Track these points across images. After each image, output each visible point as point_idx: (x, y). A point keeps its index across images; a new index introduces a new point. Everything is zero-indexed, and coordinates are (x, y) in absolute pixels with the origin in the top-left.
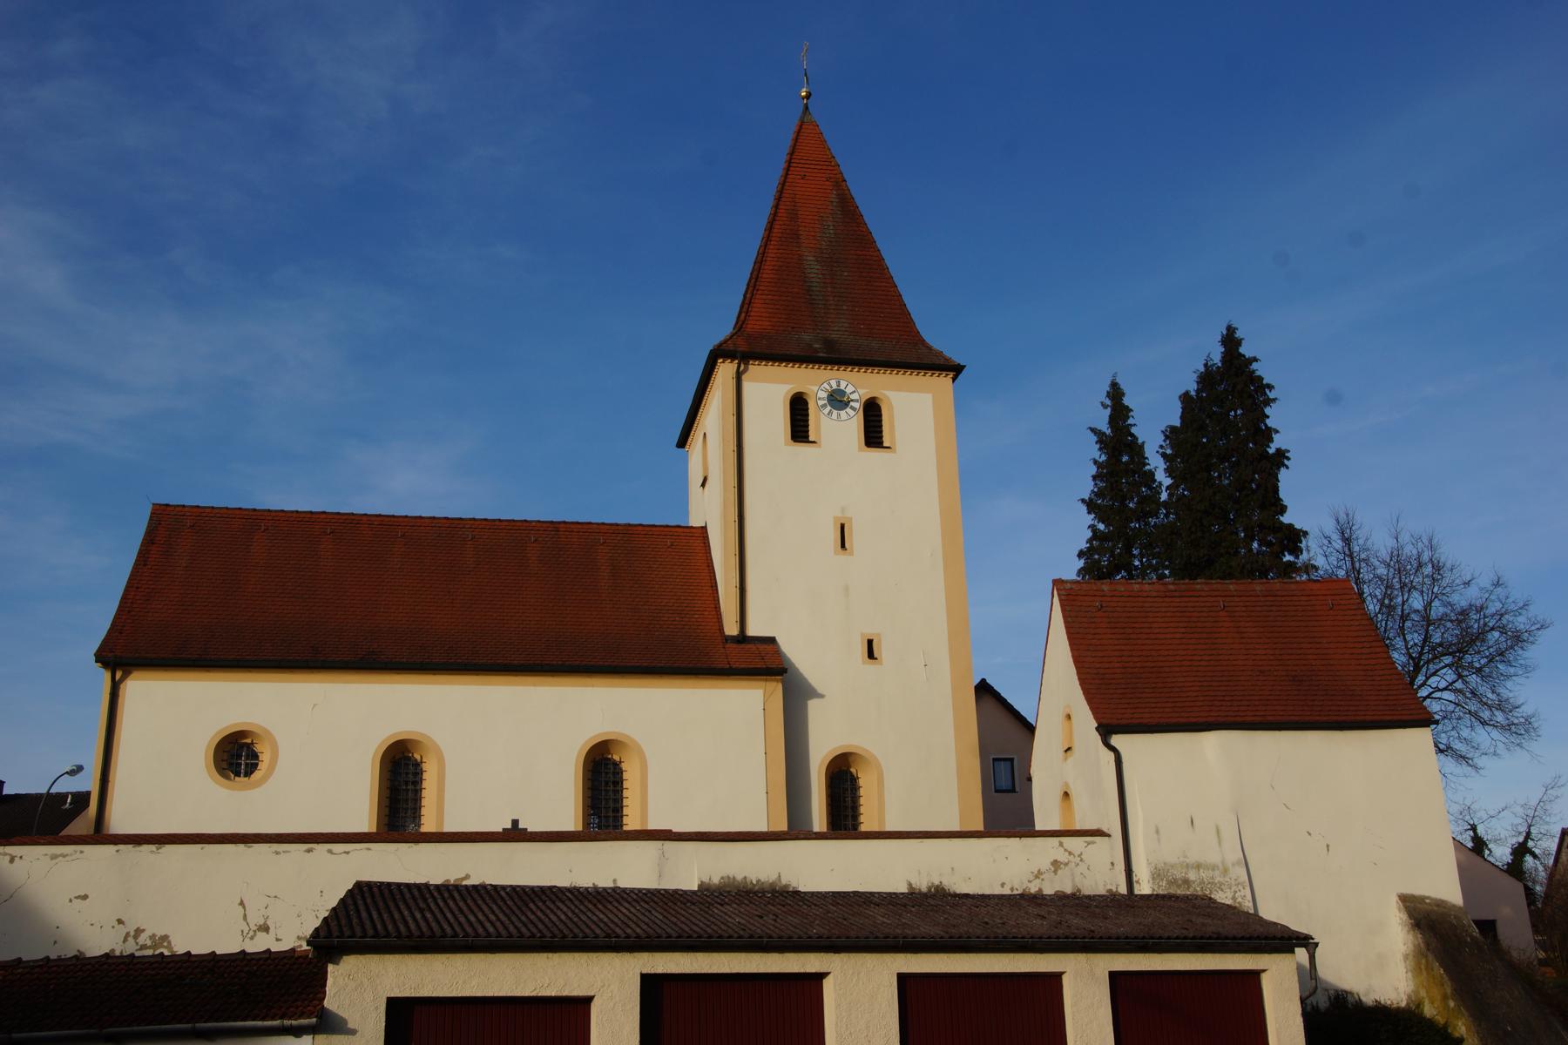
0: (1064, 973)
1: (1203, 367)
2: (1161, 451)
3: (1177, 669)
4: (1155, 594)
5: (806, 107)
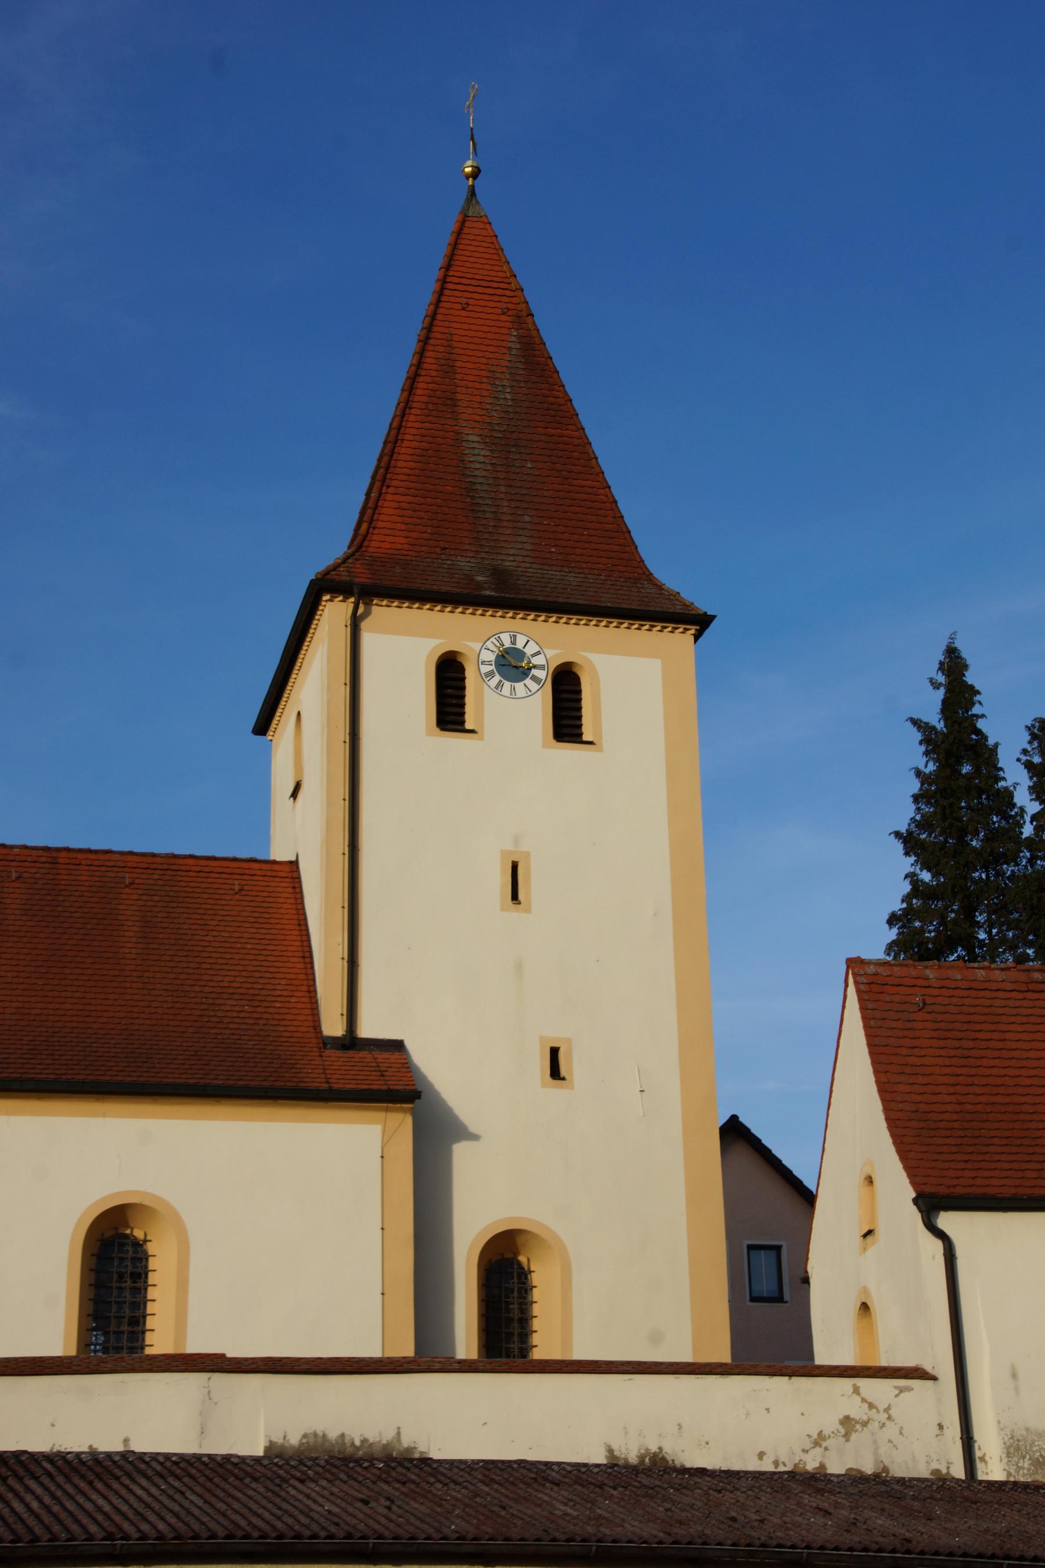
2: (1024, 758)
4: (1010, 987)
5: (472, 192)
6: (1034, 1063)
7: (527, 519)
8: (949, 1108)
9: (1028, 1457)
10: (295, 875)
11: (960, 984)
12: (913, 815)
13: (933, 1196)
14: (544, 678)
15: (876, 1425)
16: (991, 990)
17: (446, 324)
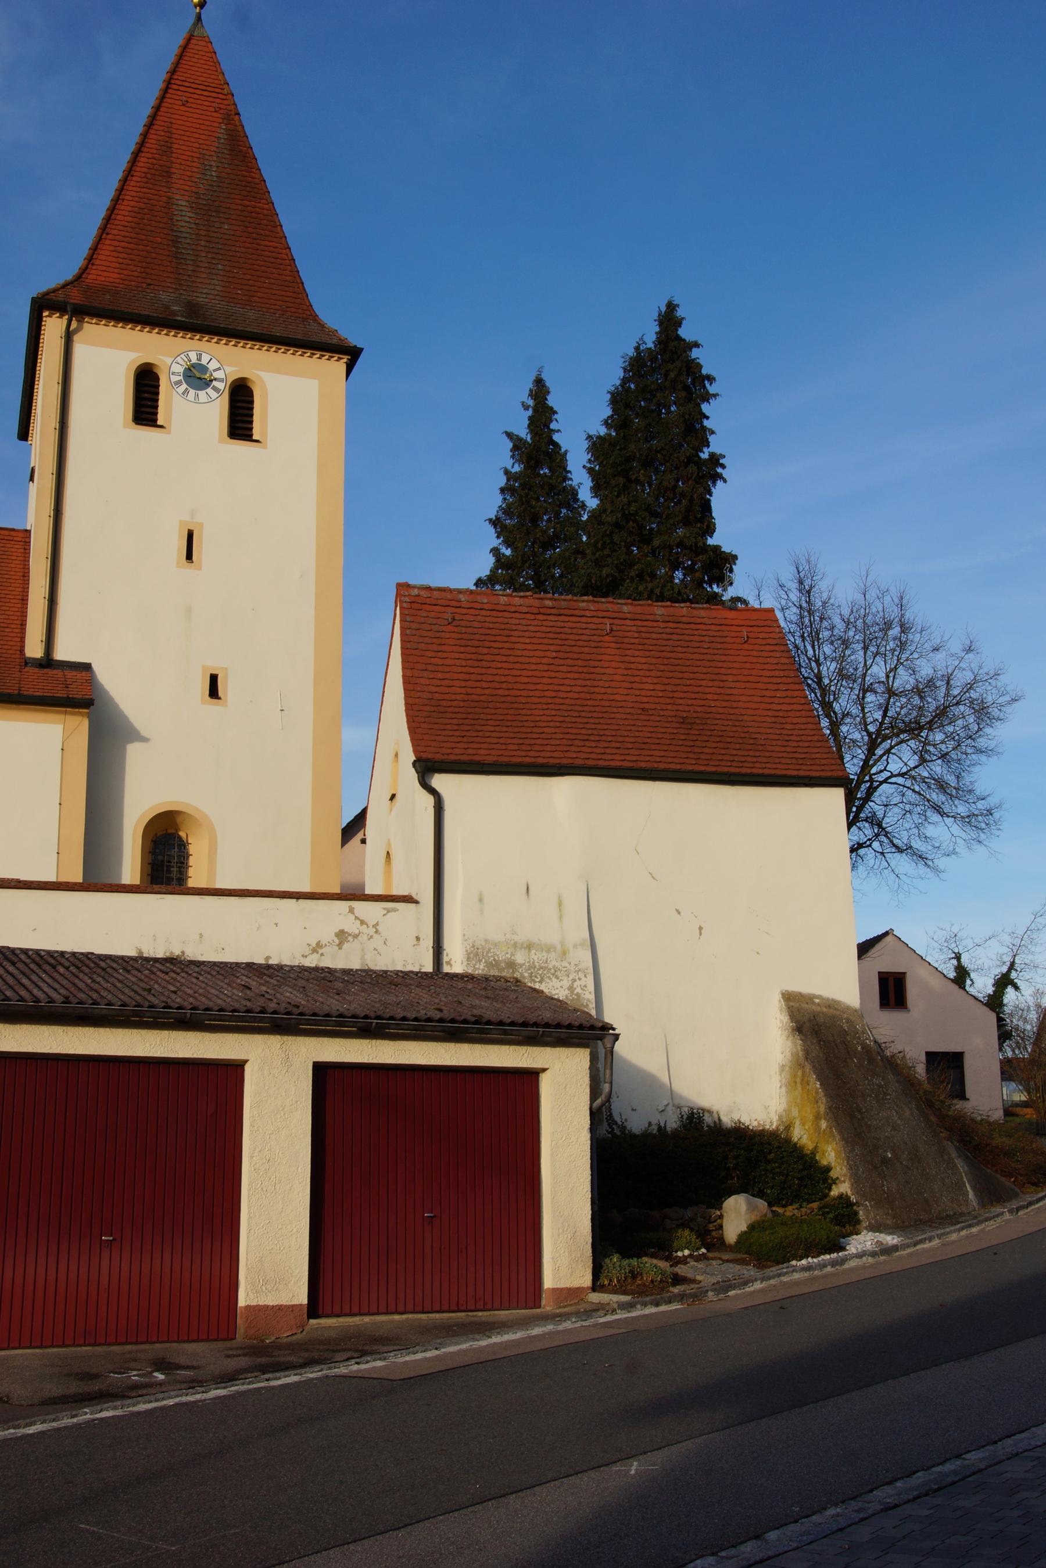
0: (246, 1061)
1: (633, 350)
2: (588, 465)
3: (537, 700)
4: (526, 610)
5: (199, 18)
6: (534, 667)
7: (220, 267)
8: (458, 697)
9: (484, 960)
10: (27, 540)
11: (485, 606)
12: (501, 504)
13: (428, 760)
14: (223, 389)
15: (365, 937)
16: (510, 612)
17: (168, 115)
